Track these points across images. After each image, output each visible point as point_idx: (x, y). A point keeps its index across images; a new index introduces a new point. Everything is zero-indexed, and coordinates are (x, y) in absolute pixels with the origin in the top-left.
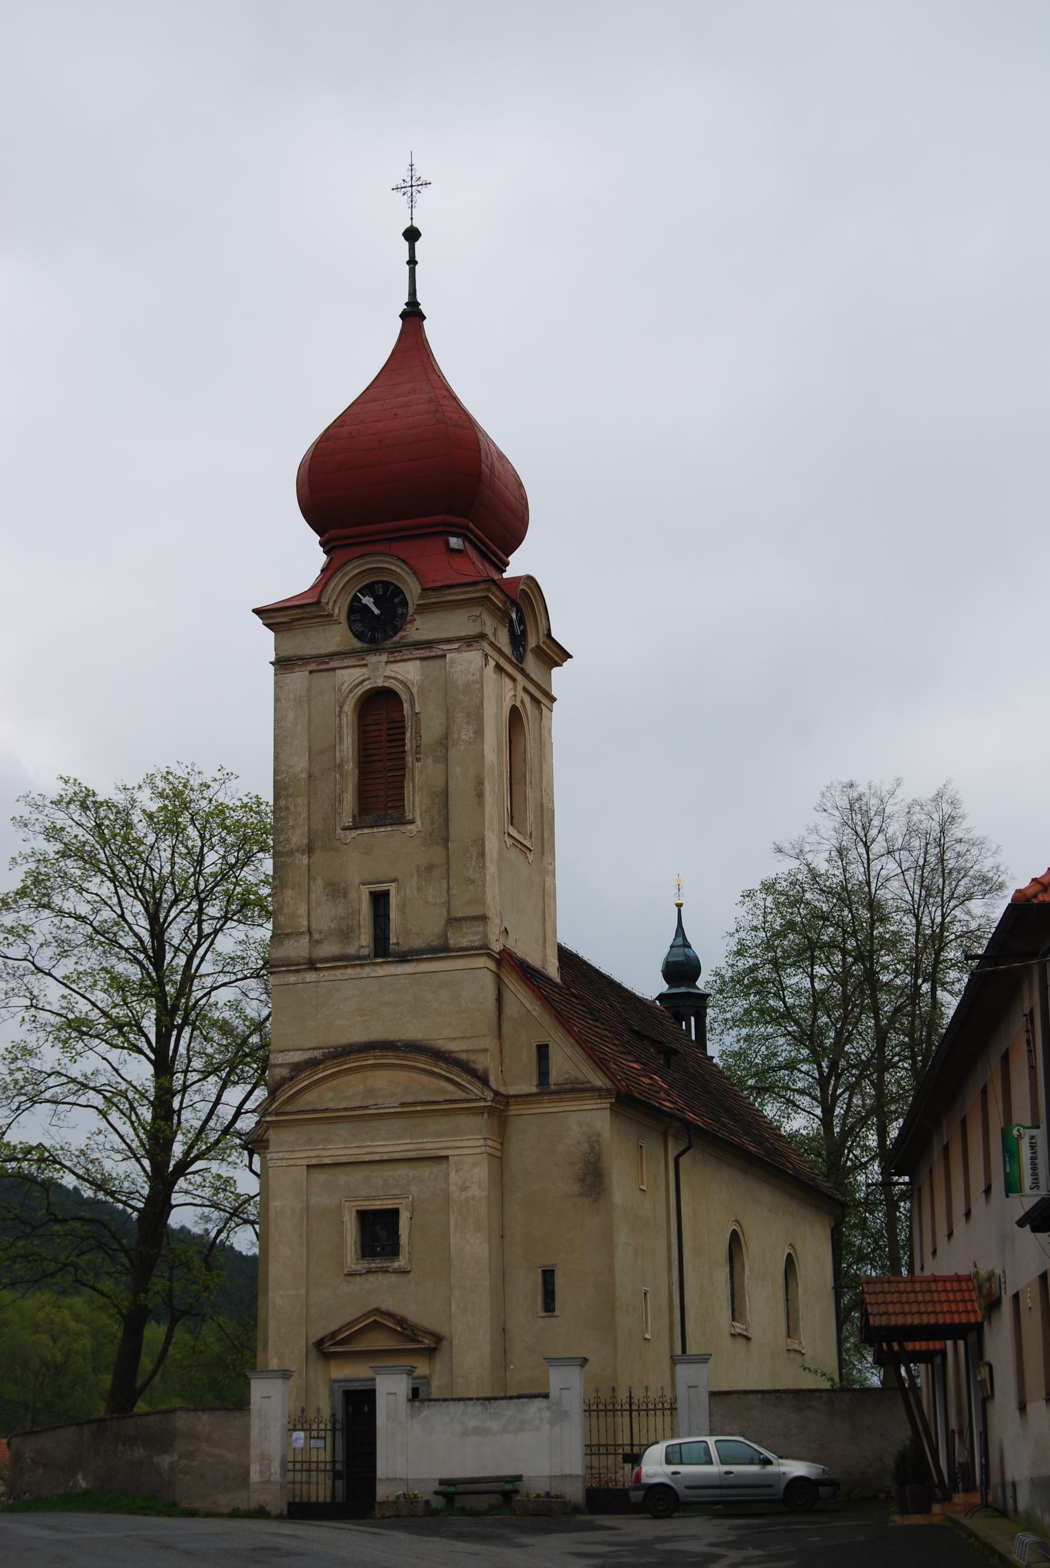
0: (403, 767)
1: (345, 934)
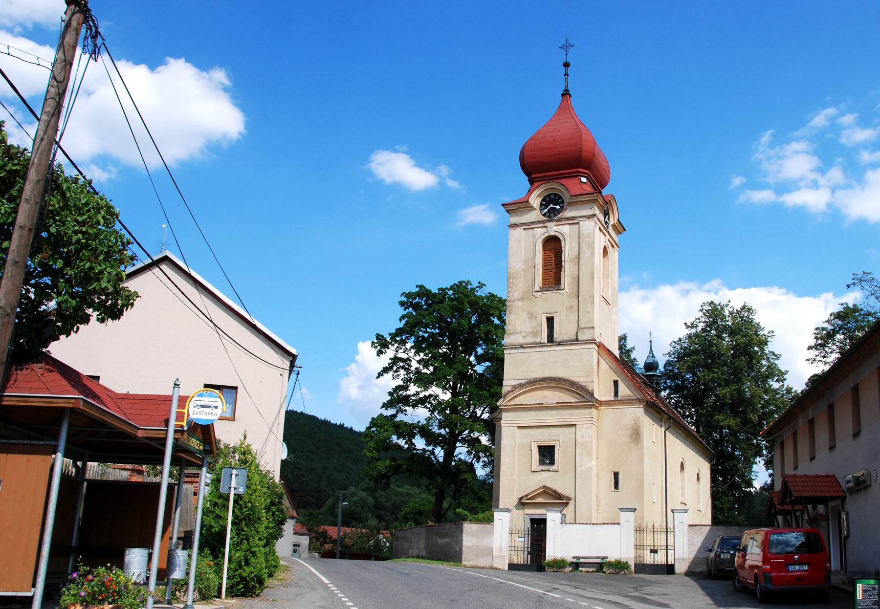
1: (535, 334)
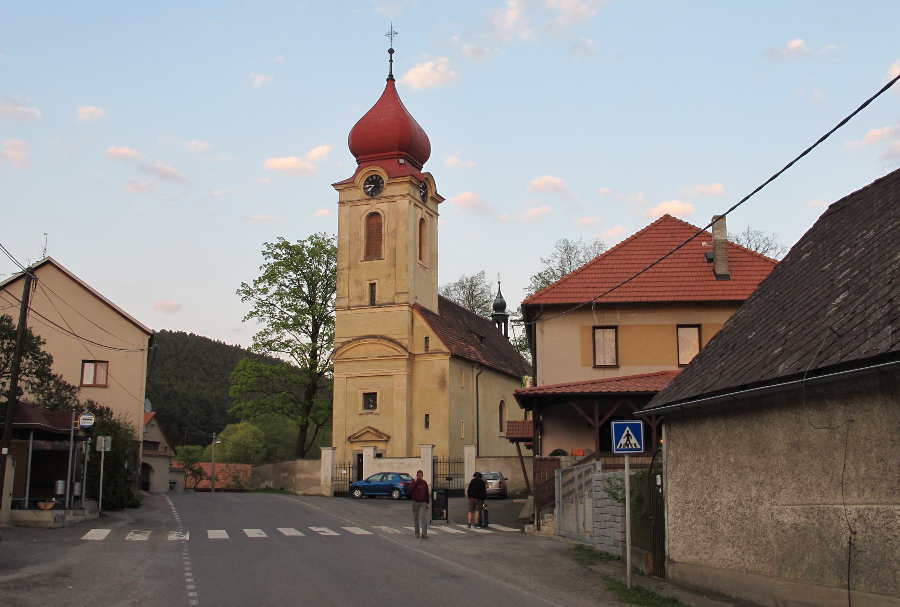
0: (381, 240)
1: (361, 298)
